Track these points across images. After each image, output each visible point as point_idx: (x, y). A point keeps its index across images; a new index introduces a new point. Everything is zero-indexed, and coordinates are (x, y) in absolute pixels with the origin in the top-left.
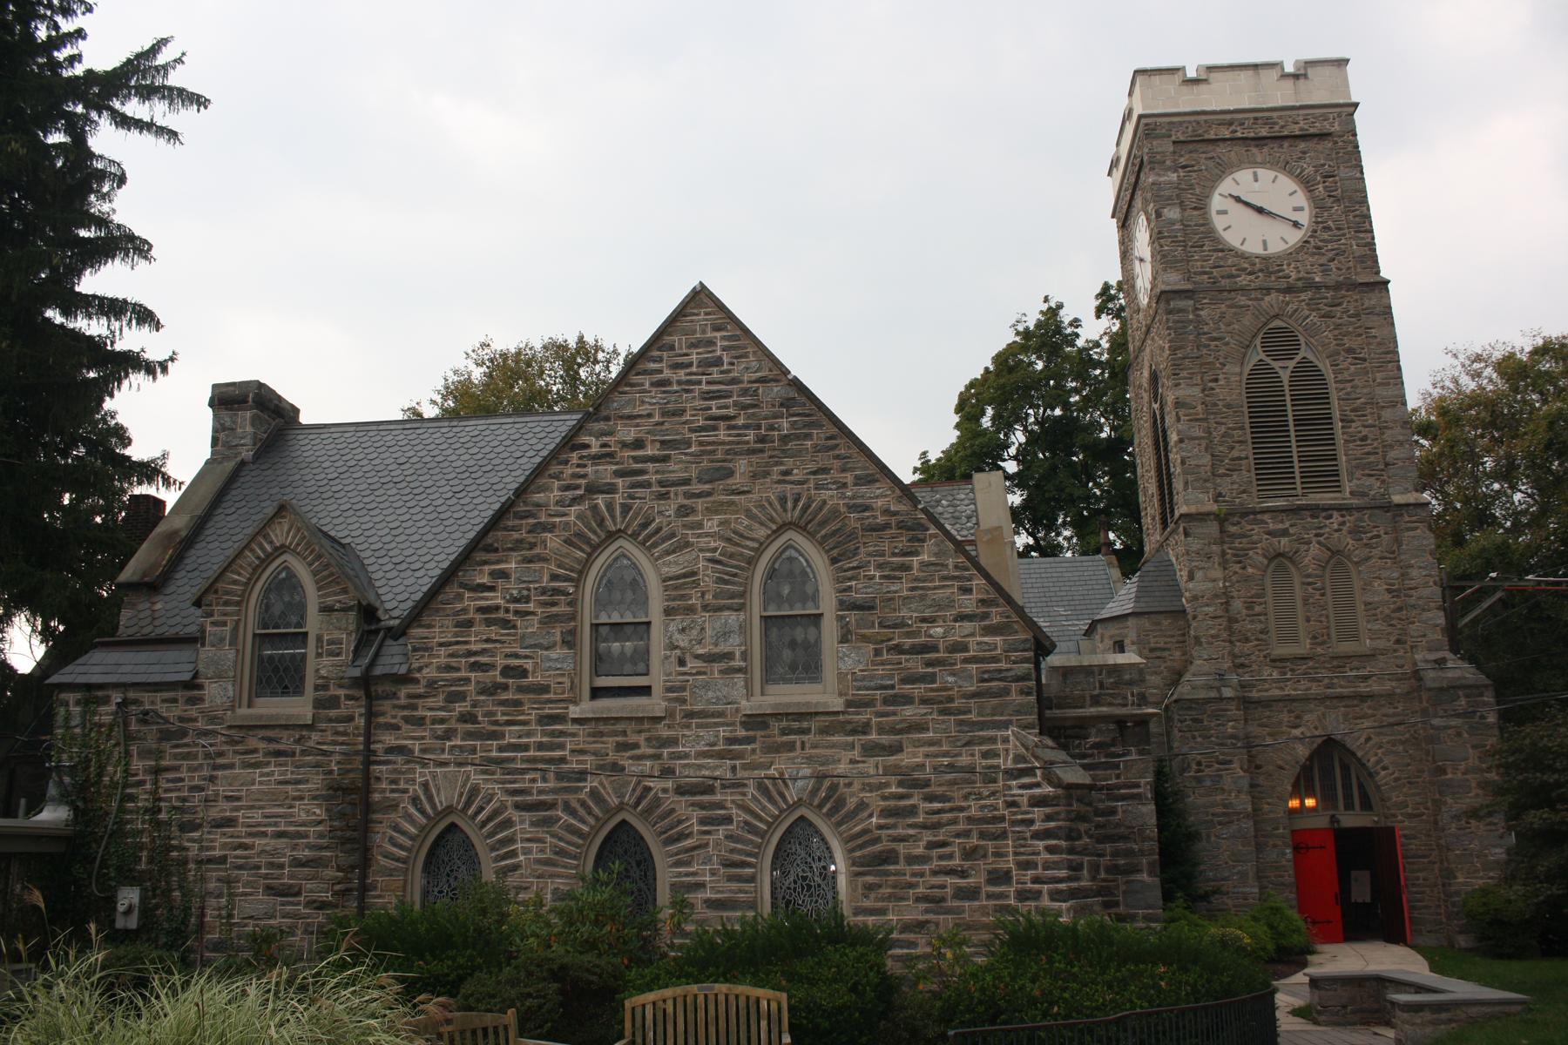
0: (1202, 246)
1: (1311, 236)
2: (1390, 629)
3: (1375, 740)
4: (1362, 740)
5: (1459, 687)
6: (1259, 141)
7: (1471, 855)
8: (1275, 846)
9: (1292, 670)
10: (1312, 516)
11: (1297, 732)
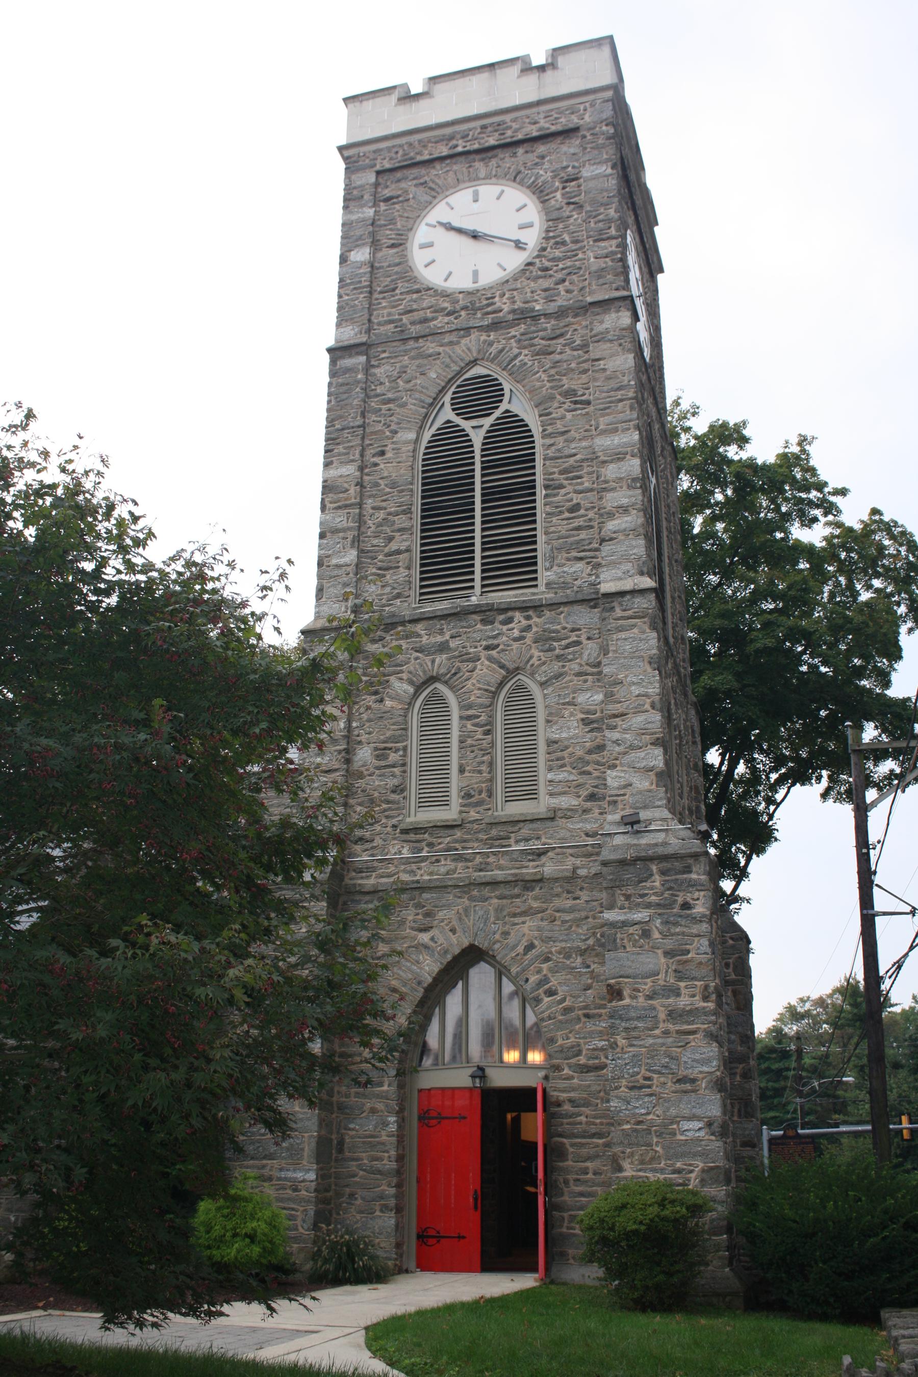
0: (394, 290)
1: (538, 256)
2: (582, 779)
3: (540, 948)
4: (520, 949)
5: (651, 859)
6: (485, 152)
7: (648, 1131)
8: (373, 1111)
9: (430, 845)
10: (484, 622)
11: (424, 937)
